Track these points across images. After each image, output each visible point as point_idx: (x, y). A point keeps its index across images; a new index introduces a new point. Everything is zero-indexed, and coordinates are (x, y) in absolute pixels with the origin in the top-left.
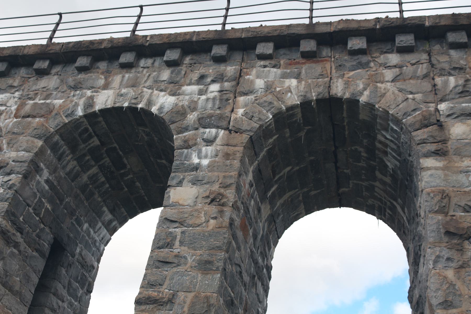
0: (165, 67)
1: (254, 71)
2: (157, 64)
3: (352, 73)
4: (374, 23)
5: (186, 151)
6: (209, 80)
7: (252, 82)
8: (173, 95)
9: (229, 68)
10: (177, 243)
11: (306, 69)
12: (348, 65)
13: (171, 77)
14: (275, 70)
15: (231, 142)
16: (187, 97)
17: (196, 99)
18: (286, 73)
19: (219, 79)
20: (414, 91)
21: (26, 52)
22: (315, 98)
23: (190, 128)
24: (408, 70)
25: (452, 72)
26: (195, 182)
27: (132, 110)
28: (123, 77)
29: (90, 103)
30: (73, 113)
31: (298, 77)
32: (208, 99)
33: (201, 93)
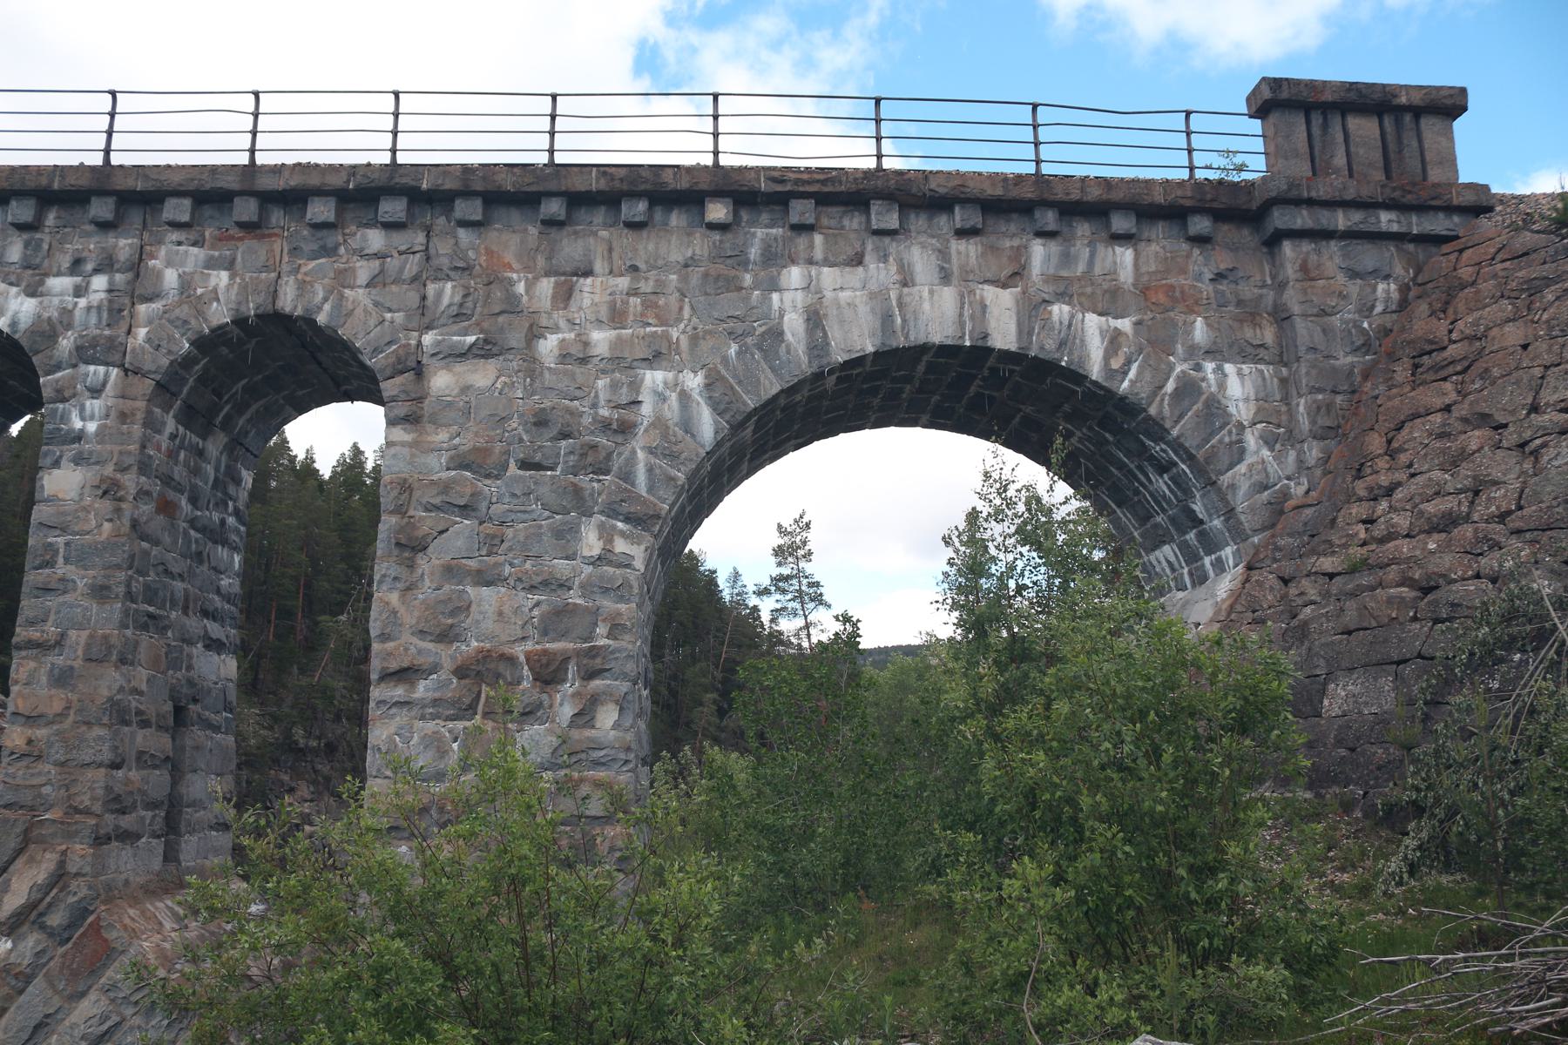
0: (12, 231)
1: (163, 252)
3: (312, 264)
4: (345, 179)
5: (61, 406)
6: (89, 267)
7: (159, 275)
9: (122, 242)
11: (243, 253)
12: (308, 247)
13: (25, 257)
14: (195, 250)
17: (70, 307)
18: (212, 257)
19: (106, 265)
20: (394, 307)
22: (252, 313)
23: (64, 365)
24: (393, 263)
25: (452, 274)
26: (79, 460)
31: (230, 266)
32: (89, 309)
33: (79, 292)
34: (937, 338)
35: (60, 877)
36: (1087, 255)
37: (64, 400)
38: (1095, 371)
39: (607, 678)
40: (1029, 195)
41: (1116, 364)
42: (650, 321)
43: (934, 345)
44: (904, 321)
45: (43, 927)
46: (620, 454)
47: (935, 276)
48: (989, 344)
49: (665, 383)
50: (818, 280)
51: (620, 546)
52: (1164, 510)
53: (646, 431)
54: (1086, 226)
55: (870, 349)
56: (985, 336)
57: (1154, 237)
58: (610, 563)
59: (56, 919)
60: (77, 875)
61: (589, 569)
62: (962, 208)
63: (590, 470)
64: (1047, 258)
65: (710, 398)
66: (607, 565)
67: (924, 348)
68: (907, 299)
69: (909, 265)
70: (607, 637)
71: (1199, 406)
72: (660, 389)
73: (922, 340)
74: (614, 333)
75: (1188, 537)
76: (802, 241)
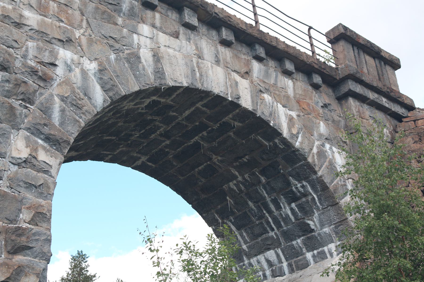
34: (216, 91)
36: (274, 76)
38: (285, 133)
39: (28, 255)
40: (256, 35)
41: (294, 132)
42: (63, 20)
43: (214, 94)
44: (201, 75)
46: (41, 94)
47: (213, 59)
48: (240, 102)
49: (72, 60)
50: (157, 37)
51: (42, 156)
52: (279, 226)
53: (60, 85)
54: (273, 62)
55: (185, 84)
56: (238, 98)
57: (298, 79)
58: (33, 167)
61: (15, 168)
62: (226, 29)
63: (21, 97)
64: (260, 71)
65: (101, 79)
66: (30, 167)
67: (207, 93)
68: (202, 66)
69: (201, 48)
70: (29, 223)
71: (326, 164)
72: (69, 62)
73: (209, 89)
74: (40, 17)
75: (294, 243)
76: (149, 13)
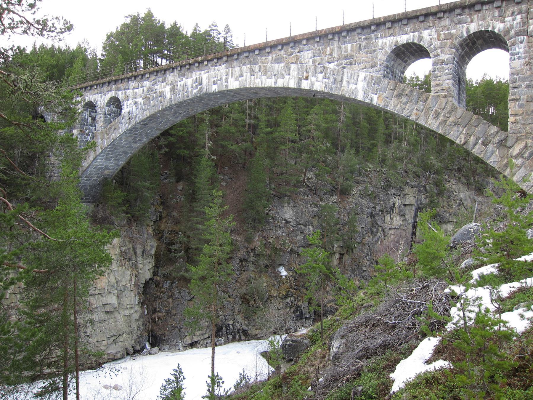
2: (491, 7)
8: (503, 23)
9: (523, 6)
10: (518, 81)
13: (499, 14)
15: (530, 41)
16: (508, 23)
19: (520, 12)
21: (432, 11)
26: (519, 58)
27: (487, 31)
28: (478, 16)
29: (468, 30)
30: (462, 36)
32: (517, 23)
33: (514, 20)
35: (526, 147)
37: (514, 45)
45: (523, 157)
59: (526, 155)
60: (530, 146)
